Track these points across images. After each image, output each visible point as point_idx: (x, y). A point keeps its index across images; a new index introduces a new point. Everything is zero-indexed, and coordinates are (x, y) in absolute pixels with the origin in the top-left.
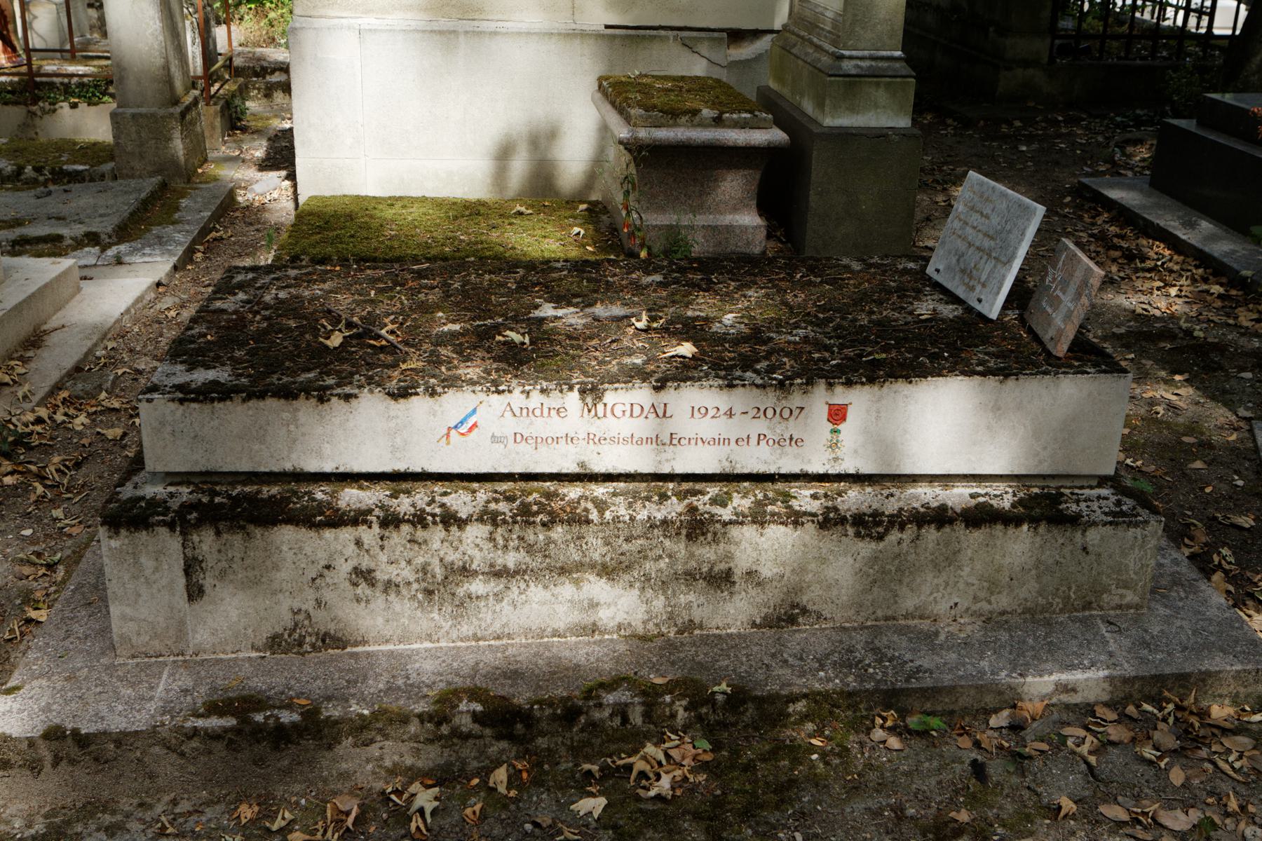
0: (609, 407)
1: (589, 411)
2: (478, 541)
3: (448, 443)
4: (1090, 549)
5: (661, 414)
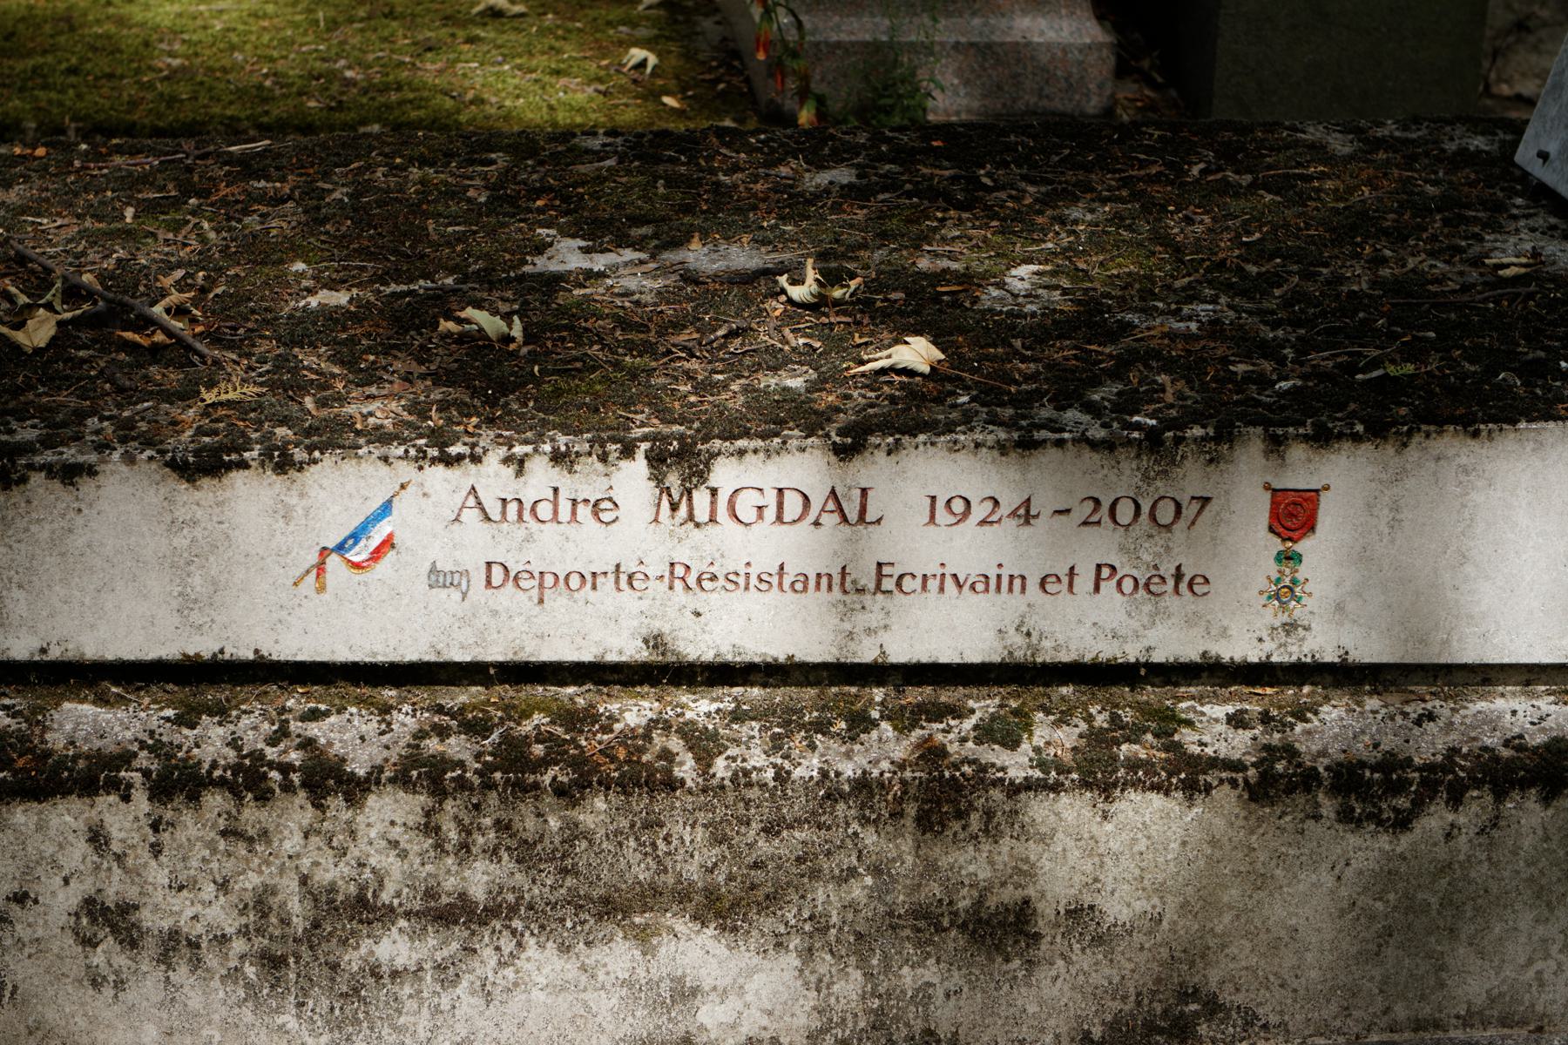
0: (723, 498)
1: (674, 507)
2: (396, 833)
5: (853, 516)
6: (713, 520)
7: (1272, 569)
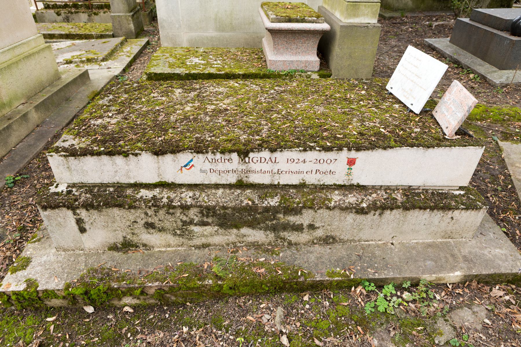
0: (251, 159)
1: (242, 160)
2: (195, 213)
3: (182, 173)
4: (454, 218)
5: (274, 161)
6: (249, 162)
7: (347, 171)
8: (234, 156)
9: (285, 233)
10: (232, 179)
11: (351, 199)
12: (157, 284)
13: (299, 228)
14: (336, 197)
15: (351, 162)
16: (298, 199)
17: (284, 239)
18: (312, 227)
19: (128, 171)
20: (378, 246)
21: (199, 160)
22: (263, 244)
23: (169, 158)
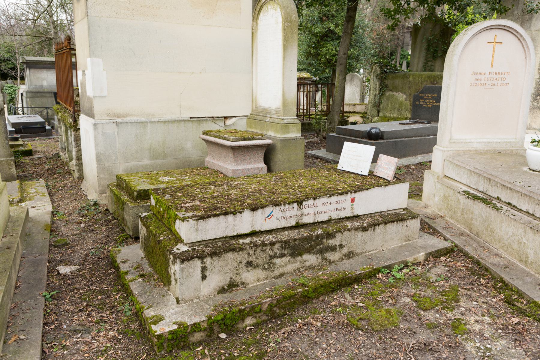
8: (295, 205)
9: (327, 254)
10: (293, 223)
11: (357, 224)
12: (269, 299)
13: (333, 249)
14: (349, 224)
15: (353, 200)
16: (330, 229)
17: (326, 259)
18: (341, 246)
19: (234, 226)
20: (377, 253)
21: (277, 211)
22: (315, 267)
23: (260, 211)
